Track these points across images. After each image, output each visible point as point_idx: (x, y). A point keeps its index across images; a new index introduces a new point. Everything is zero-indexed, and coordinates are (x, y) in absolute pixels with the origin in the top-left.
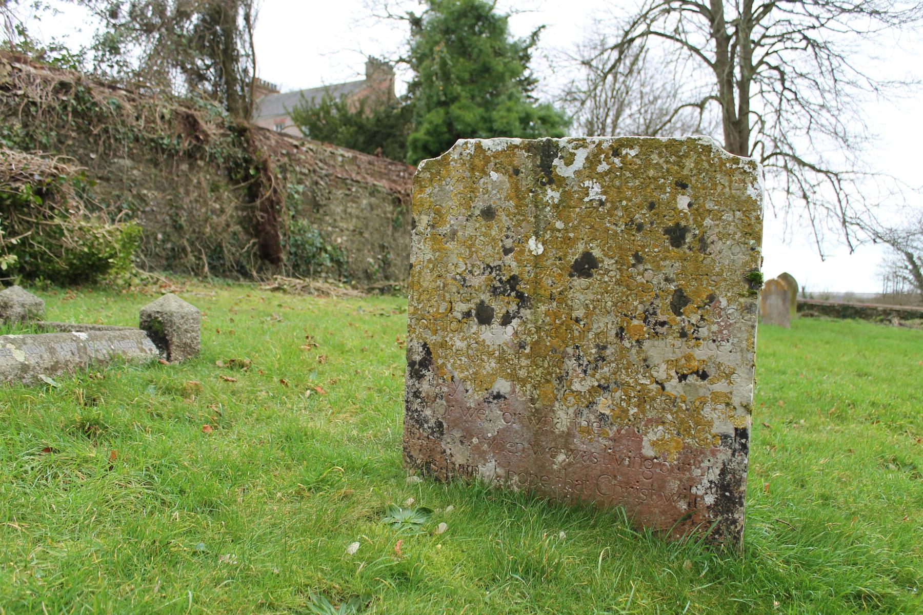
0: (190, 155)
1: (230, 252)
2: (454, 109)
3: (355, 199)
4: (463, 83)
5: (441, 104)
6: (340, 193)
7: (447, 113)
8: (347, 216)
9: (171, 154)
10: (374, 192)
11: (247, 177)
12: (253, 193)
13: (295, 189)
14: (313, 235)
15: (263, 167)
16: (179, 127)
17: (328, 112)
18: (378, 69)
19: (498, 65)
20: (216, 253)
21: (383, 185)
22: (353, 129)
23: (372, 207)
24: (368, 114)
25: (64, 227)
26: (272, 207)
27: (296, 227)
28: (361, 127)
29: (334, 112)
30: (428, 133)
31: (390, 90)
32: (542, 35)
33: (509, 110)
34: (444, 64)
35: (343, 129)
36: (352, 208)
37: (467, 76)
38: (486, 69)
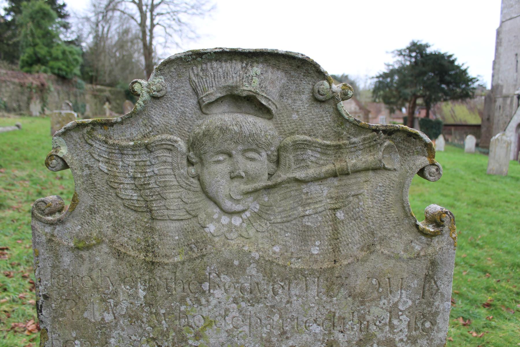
2: (37, 49)
4: (39, 38)
7: (34, 50)
8: (7, 92)
10: (14, 83)
21: (16, 81)
23: (14, 88)
30: (28, 57)
34: (31, 31)
36: (8, 89)
37: (40, 36)
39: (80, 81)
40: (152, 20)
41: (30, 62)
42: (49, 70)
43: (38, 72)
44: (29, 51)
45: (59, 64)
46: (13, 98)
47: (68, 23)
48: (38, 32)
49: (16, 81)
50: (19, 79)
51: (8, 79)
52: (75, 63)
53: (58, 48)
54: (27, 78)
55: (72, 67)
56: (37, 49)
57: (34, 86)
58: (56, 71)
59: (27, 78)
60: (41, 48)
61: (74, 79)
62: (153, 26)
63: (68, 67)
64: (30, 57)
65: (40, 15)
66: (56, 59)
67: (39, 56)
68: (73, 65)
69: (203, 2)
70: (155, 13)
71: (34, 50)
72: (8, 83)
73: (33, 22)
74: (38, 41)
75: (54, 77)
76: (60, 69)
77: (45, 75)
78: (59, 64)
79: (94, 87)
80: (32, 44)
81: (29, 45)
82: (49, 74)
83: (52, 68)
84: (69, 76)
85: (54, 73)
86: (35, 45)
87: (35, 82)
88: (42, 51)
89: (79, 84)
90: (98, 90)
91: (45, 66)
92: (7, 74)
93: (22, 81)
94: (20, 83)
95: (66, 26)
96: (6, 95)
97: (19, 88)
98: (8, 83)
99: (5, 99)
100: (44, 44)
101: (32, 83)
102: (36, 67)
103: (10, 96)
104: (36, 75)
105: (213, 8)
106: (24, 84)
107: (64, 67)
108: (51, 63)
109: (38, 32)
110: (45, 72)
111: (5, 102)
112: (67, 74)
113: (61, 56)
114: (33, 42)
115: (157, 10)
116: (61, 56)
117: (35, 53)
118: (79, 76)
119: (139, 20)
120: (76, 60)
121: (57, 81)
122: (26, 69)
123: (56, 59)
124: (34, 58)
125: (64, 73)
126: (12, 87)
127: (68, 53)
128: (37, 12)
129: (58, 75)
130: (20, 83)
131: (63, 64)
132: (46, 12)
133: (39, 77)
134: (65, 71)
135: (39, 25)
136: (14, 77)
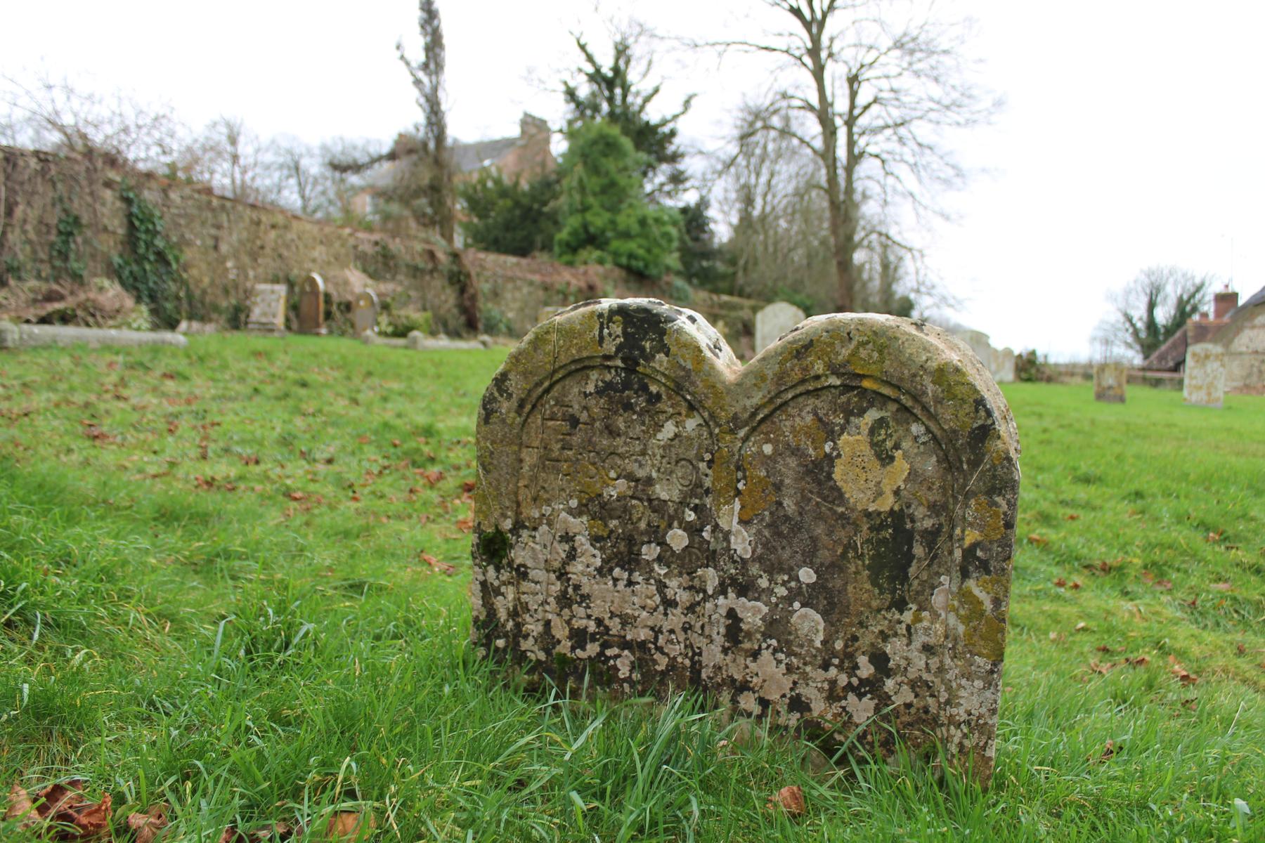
0: (431, 272)
1: (452, 324)
2: (589, 217)
3: (519, 289)
4: (595, 194)
5: (578, 211)
6: (510, 286)
7: (584, 218)
8: (514, 300)
9: (422, 271)
10: (531, 283)
11: (459, 281)
12: (463, 291)
13: (485, 287)
14: (495, 312)
15: (468, 276)
16: (426, 257)
17: (484, 185)
18: (534, 128)
19: (622, 181)
20: (445, 325)
21: (537, 278)
22: (509, 203)
23: (530, 293)
24: (525, 186)
25: (1184, 328)
26: (473, 298)
27: (486, 307)
28: (517, 204)
29: (490, 184)
30: (570, 234)
31: (547, 152)
32: (693, 102)
33: (629, 216)
34: (581, 181)
35: (501, 202)
36: (517, 295)
37: (597, 189)
38: (613, 184)
39: (679, 282)
40: (851, 143)
41: (574, 244)
42: (609, 259)
43: (585, 263)
44: (573, 222)
45: (632, 246)
46: (527, 311)
47: (682, 173)
48: (594, 183)
49: (537, 278)
50: (543, 275)
51: (519, 274)
52: (664, 243)
53: (630, 211)
54: (559, 274)
55: (656, 251)
56: (589, 217)
57: (573, 289)
58: (624, 260)
59: (559, 274)
60: (597, 214)
61: (665, 278)
62: (855, 158)
63: (649, 251)
64: (574, 233)
65: (601, 147)
66: (626, 235)
67: (592, 230)
68: (659, 246)
69: (857, 3)
70: (855, 129)
71: (584, 218)
72: (519, 283)
73: (585, 163)
74: (591, 200)
75: (618, 273)
76: (631, 256)
77: (600, 269)
78: (632, 246)
79: (715, 297)
80: (579, 207)
81: (573, 211)
82: (609, 266)
83: (616, 254)
84: (653, 271)
85: (620, 266)
86: (585, 209)
87: (574, 281)
88: (598, 220)
89: (678, 289)
90: (723, 306)
91: (602, 250)
92: (518, 264)
93: (548, 280)
94: (543, 282)
95: (677, 179)
96: (512, 305)
97: (541, 293)
98: (519, 283)
99: (510, 315)
100: (603, 206)
101: (568, 284)
102: (584, 254)
103: (522, 310)
104: (582, 269)
105: (999, 104)
106: (552, 285)
107: (641, 252)
108: (615, 244)
109: (594, 183)
110: (601, 262)
111: (509, 320)
112: (646, 266)
113: (635, 228)
114: (582, 203)
115: (863, 121)
116: (635, 228)
117: (585, 226)
118: (678, 273)
119: (818, 144)
120: (666, 235)
121: (626, 281)
122: (566, 258)
123: (626, 235)
124: (583, 236)
125: (641, 264)
126: (525, 290)
127: (650, 221)
128: (594, 143)
129: (629, 269)
130: (543, 282)
131: (640, 246)
132: (611, 140)
133: (585, 273)
134: (643, 259)
135: (595, 170)
136: (533, 272)
